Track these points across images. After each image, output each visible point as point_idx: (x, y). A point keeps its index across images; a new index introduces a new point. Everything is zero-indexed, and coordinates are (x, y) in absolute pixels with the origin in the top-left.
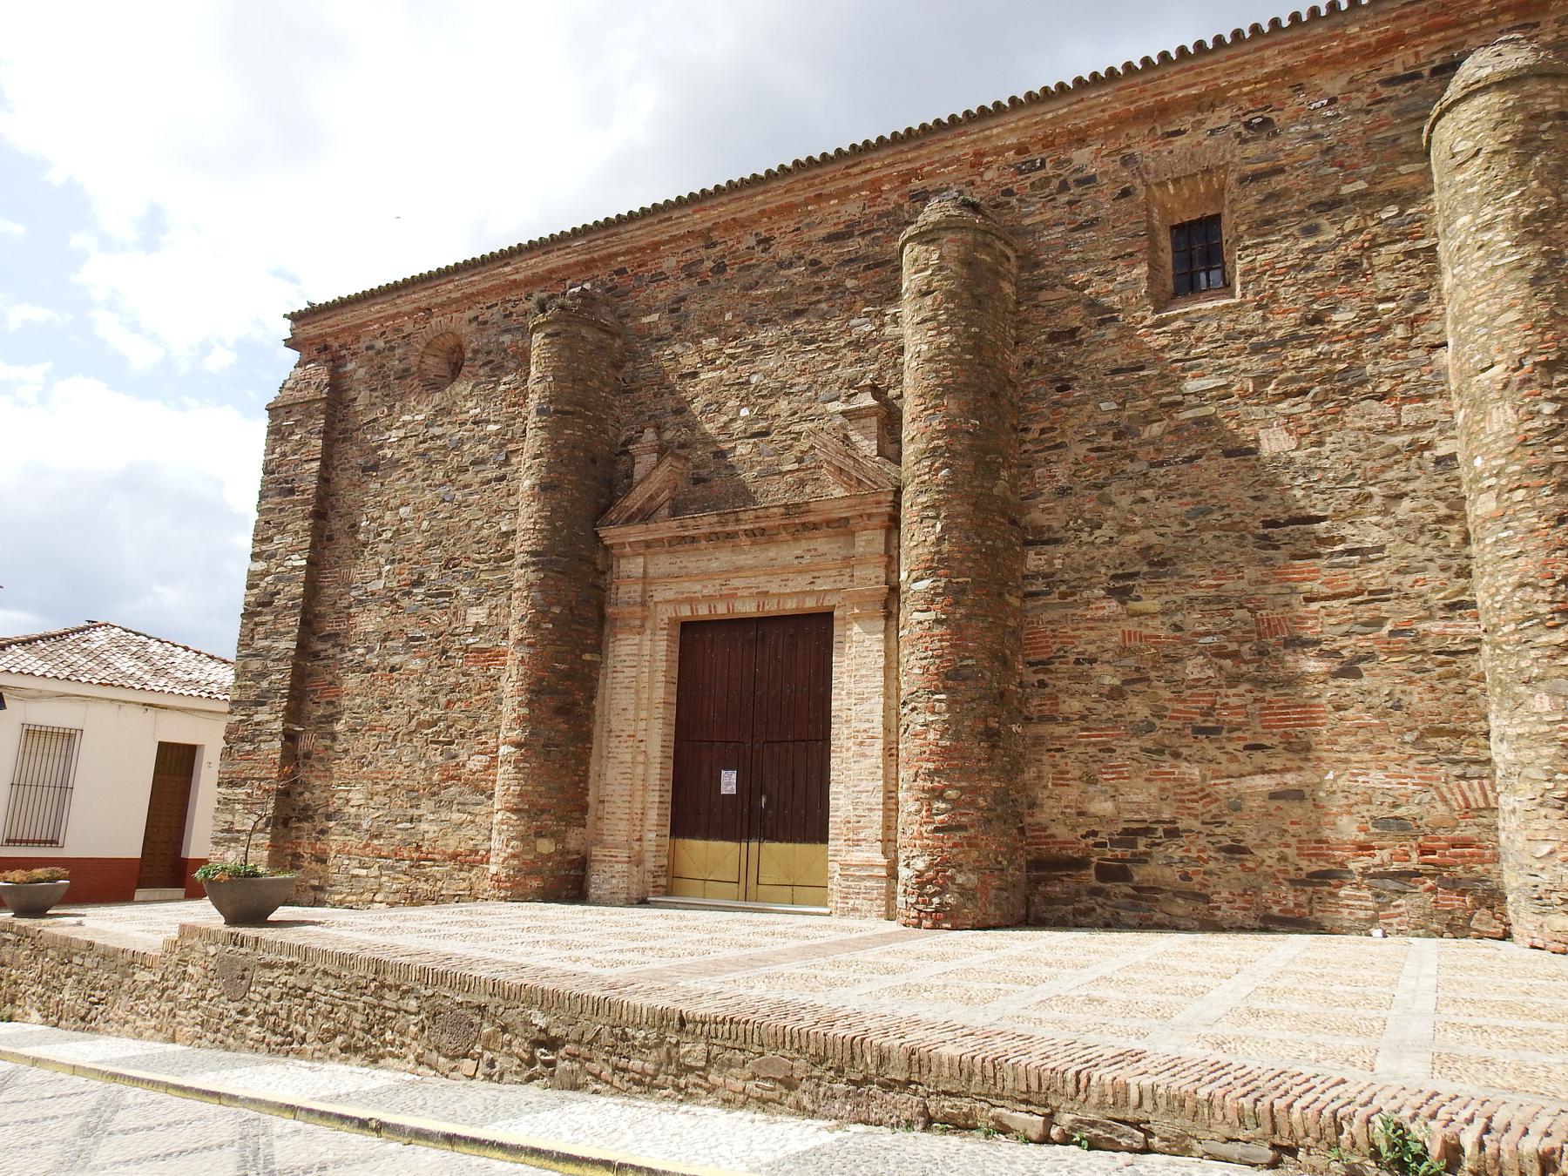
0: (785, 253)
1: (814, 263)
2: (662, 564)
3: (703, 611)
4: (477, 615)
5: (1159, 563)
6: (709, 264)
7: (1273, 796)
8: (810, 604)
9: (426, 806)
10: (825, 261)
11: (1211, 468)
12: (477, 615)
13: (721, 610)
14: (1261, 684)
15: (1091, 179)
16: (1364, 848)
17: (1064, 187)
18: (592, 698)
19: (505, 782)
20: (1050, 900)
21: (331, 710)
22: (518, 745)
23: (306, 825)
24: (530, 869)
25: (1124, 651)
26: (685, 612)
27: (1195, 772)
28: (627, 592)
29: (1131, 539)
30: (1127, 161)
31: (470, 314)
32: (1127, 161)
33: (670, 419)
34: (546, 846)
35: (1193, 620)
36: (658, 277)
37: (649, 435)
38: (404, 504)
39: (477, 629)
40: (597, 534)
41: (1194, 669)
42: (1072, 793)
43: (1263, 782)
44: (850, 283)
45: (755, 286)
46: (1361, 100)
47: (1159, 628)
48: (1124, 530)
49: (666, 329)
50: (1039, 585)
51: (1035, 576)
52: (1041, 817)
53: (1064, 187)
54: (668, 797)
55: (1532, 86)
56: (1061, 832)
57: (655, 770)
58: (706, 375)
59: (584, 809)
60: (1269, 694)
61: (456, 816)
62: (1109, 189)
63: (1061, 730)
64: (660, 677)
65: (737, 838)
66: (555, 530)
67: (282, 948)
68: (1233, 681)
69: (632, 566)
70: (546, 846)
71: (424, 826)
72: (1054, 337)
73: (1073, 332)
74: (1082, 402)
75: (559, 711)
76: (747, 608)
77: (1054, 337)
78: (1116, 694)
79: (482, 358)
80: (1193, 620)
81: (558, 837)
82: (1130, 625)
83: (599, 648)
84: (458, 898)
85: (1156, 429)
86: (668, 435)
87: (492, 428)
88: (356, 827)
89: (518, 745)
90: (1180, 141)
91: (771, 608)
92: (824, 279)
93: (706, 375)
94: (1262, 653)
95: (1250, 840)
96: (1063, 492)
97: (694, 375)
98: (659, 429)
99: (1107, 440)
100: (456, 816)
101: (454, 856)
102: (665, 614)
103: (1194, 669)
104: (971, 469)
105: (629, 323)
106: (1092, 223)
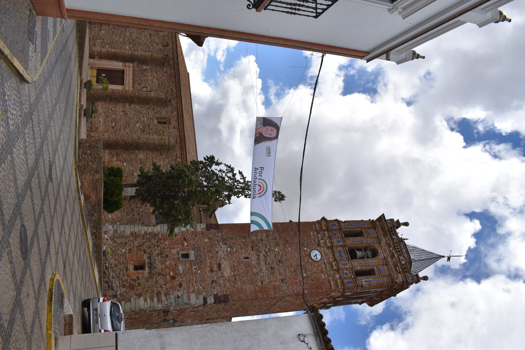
0: (171, 84)
1: (169, 87)
2: (131, 69)
3: (125, 73)
4: (127, 47)
5: (126, 115)
6: (171, 76)
7: (100, 121)
8: (125, 83)
9: (101, 41)
10: (169, 88)
11: (136, 120)
12: (127, 47)
13: (125, 75)
14: (112, 121)
15: (172, 113)
16: (94, 127)
17: (172, 111)
18: (115, 60)
19: (104, 50)
20: (89, 102)
21: (116, 29)
22: (108, 51)
23: (99, 25)
24: (93, 51)
25: (116, 111)
26: (125, 71)
27: (103, 115)
28: (127, 64)
29: (129, 113)
30: (174, 117)
31: (171, 48)
32: (174, 117)
33: (151, 70)
34: (96, 54)
35: (119, 117)
36: (171, 70)
37: (149, 68)
38: (144, 39)
39: (125, 47)
40: (135, 61)
41: (114, 116)
42: (101, 105)
43: (101, 120)
44: (165, 90)
45: (167, 80)
46: (175, 136)
47: (118, 114)
48: (130, 112)
49: (163, 71)
50: (124, 104)
51: (126, 104)
52: (98, 102)
53: (172, 111)
54: (102, 68)
55: (168, 141)
56: (97, 104)
57: (105, 67)
58: (156, 75)
59: (101, 59)
60: (110, 121)
61: (100, 44)
62: (170, 115)
63: (108, 105)
64: (117, 68)
65: (97, 75)
66: (471, 145)
67: (86, 25)
68: (112, 119)
69: (131, 65)
70: (96, 54)
71: (99, 40)
72: (154, 108)
73: (154, 110)
74: (145, 110)
75: (113, 56)
76: (125, 77)
77: (154, 108)
78: (111, 110)
79: (164, 49)
80: (119, 117)
81: (97, 55)
82: (119, 111)
83: (121, 61)
84: (90, 44)
85: (141, 116)
86: (149, 70)
87: (154, 50)
88: (99, 32)
89: (108, 51)
90: (175, 121)
91: (125, 80)
92: (166, 88)
93: (156, 75)
94: (115, 121)
95: (95, 118)
96: (135, 107)
97: (156, 74)
98: (150, 69)
99: (140, 112)
100: (100, 44)
101: (95, 44)
102: (125, 69)
103: (114, 116)
104: (159, 152)
105: (165, 67)
106: (167, 113)
